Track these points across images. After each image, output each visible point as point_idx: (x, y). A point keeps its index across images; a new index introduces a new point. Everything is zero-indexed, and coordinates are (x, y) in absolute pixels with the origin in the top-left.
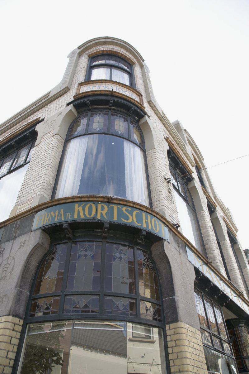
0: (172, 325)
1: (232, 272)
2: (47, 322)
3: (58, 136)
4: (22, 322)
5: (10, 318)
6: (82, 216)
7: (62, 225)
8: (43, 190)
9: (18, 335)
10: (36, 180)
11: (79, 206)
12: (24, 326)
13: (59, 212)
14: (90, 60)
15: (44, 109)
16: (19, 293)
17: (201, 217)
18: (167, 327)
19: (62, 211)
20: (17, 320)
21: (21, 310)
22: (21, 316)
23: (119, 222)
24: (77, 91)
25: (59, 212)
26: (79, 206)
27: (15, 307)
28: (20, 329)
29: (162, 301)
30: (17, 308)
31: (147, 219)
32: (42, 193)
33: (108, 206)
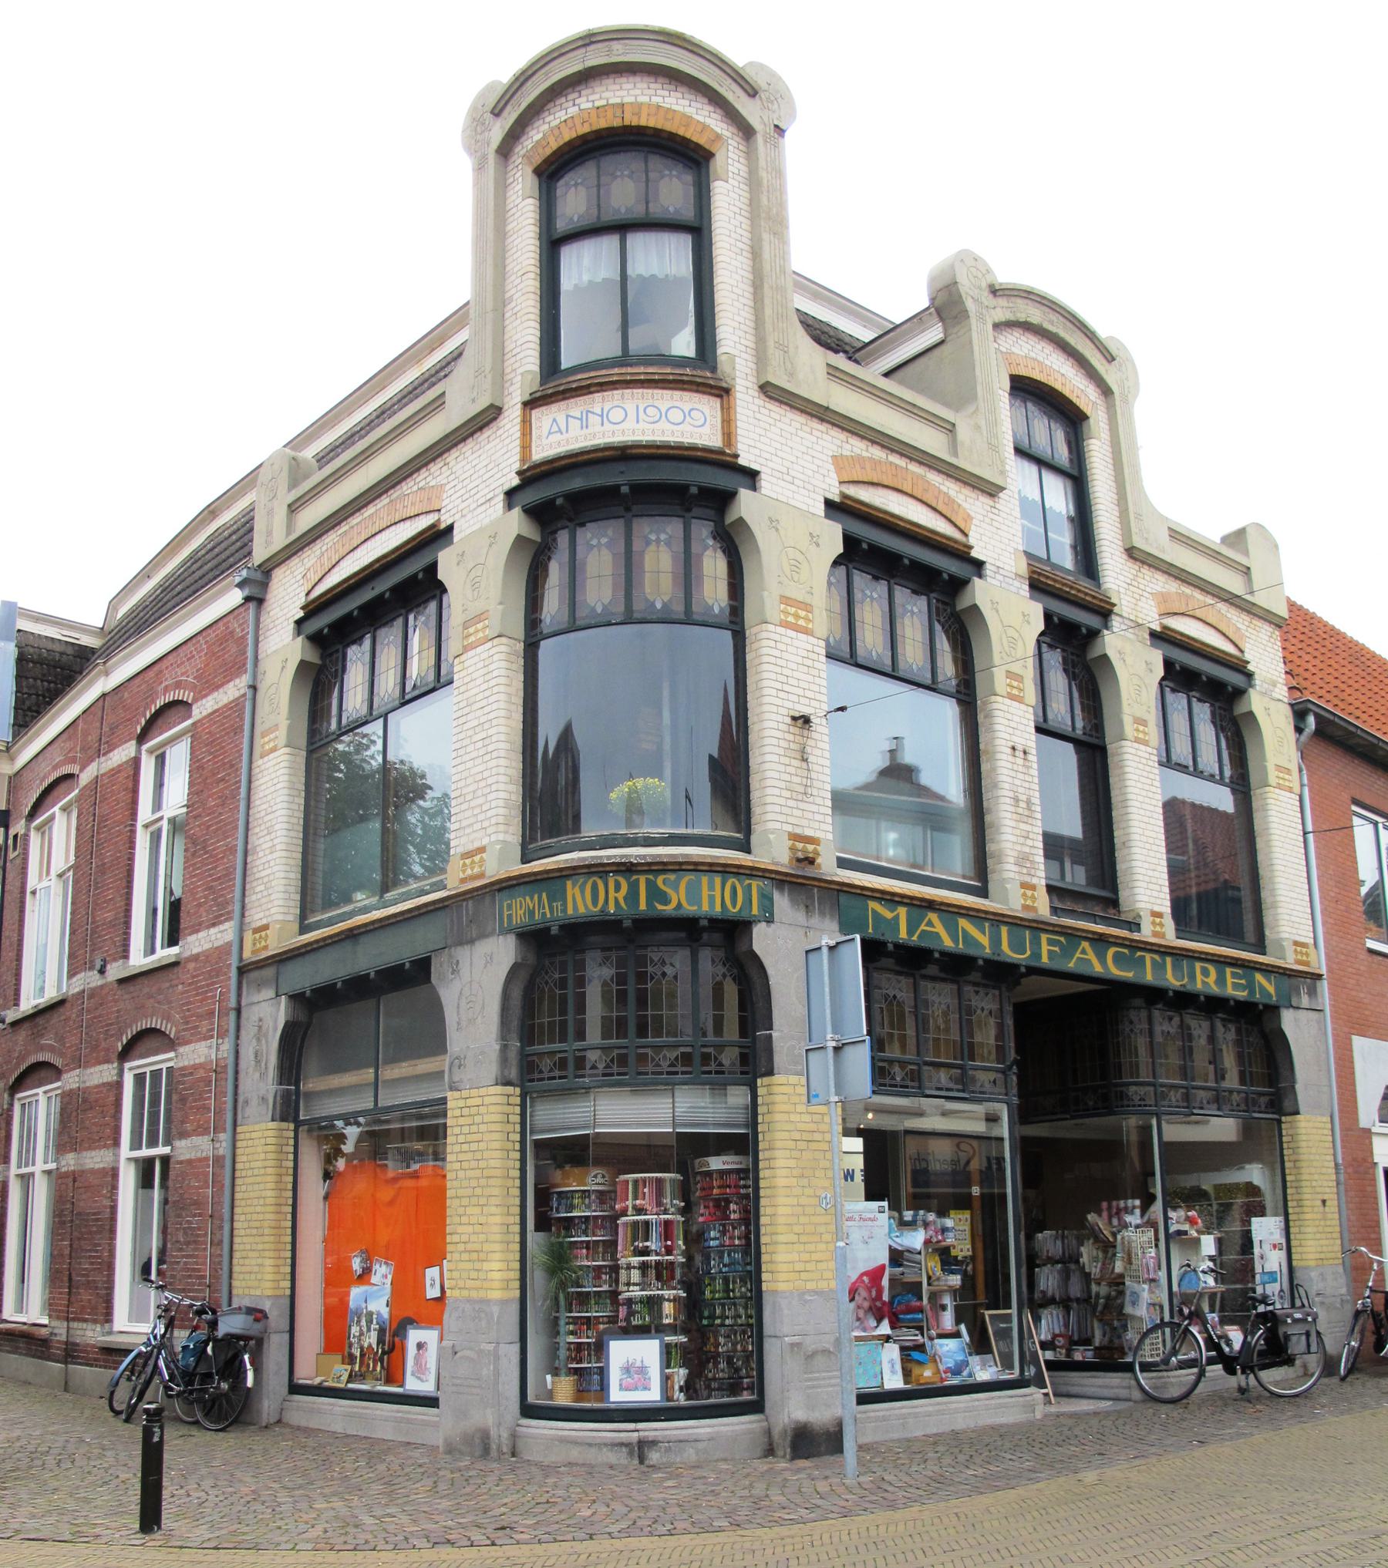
0: (766, 1080)
1: (1125, 851)
2: (1085, 326)
3: (504, 640)
4: (518, 1090)
5: (499, 1089)
6: (582, 910)
7: (548, 929)
8: (502, 828)
9: (518, 1110)
10: (477, 826)
11: (574, 886)
12: (523, 1096)
13: (540, 898)
14: (544, 185)
15: (434, 468)
16: (504, 1049)
17: (986, 717)
18: (759, 1081)
19: (544, 895)
20: (510, 1089)
21: (513, 1073)
22: (515, 1081)
23: (652, 914)
24: (523, 460)
25: (540, 898)
26: (574, 886)
27: (502, 1072)
28: (518, 1100)
29: (754, 1038)
30: (506, 1073)
31: (711, 888)
32: (501, 837)
33: (627, 880)
